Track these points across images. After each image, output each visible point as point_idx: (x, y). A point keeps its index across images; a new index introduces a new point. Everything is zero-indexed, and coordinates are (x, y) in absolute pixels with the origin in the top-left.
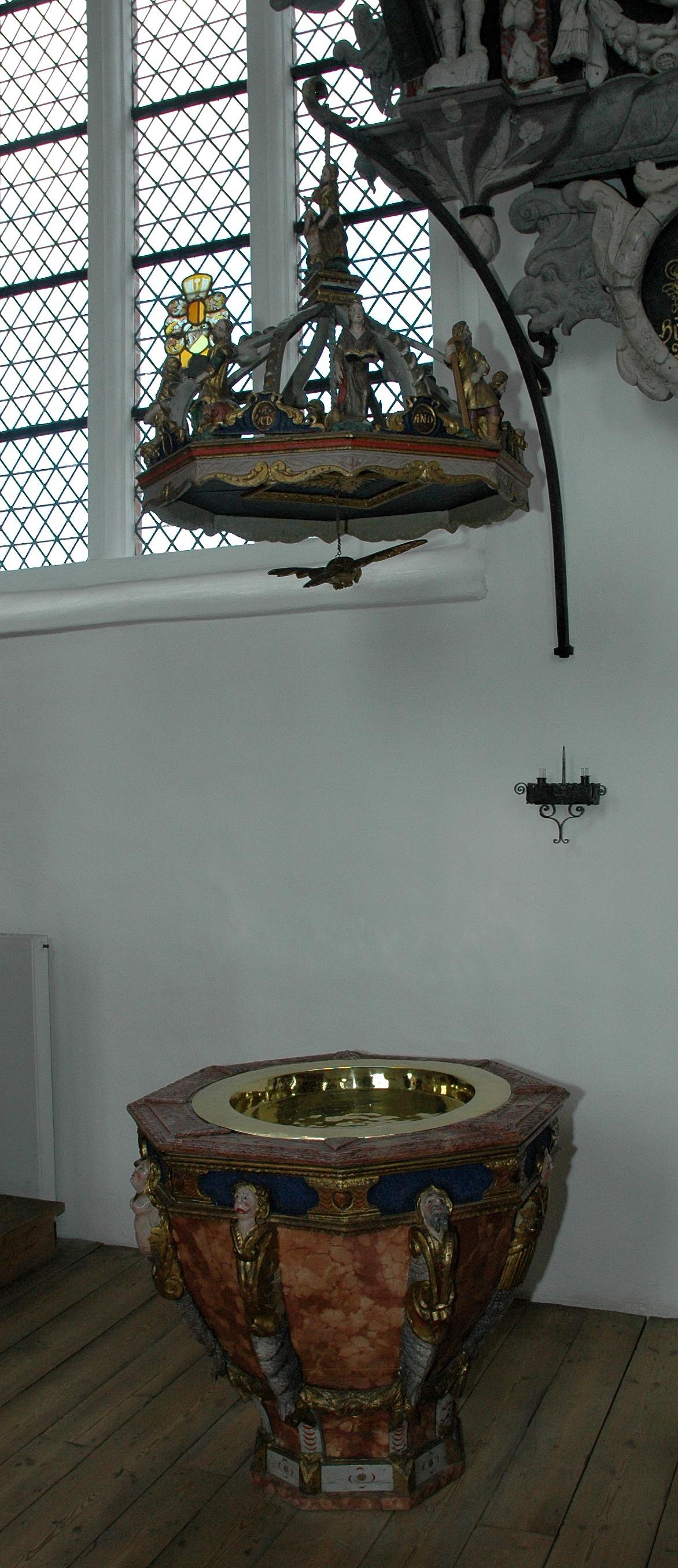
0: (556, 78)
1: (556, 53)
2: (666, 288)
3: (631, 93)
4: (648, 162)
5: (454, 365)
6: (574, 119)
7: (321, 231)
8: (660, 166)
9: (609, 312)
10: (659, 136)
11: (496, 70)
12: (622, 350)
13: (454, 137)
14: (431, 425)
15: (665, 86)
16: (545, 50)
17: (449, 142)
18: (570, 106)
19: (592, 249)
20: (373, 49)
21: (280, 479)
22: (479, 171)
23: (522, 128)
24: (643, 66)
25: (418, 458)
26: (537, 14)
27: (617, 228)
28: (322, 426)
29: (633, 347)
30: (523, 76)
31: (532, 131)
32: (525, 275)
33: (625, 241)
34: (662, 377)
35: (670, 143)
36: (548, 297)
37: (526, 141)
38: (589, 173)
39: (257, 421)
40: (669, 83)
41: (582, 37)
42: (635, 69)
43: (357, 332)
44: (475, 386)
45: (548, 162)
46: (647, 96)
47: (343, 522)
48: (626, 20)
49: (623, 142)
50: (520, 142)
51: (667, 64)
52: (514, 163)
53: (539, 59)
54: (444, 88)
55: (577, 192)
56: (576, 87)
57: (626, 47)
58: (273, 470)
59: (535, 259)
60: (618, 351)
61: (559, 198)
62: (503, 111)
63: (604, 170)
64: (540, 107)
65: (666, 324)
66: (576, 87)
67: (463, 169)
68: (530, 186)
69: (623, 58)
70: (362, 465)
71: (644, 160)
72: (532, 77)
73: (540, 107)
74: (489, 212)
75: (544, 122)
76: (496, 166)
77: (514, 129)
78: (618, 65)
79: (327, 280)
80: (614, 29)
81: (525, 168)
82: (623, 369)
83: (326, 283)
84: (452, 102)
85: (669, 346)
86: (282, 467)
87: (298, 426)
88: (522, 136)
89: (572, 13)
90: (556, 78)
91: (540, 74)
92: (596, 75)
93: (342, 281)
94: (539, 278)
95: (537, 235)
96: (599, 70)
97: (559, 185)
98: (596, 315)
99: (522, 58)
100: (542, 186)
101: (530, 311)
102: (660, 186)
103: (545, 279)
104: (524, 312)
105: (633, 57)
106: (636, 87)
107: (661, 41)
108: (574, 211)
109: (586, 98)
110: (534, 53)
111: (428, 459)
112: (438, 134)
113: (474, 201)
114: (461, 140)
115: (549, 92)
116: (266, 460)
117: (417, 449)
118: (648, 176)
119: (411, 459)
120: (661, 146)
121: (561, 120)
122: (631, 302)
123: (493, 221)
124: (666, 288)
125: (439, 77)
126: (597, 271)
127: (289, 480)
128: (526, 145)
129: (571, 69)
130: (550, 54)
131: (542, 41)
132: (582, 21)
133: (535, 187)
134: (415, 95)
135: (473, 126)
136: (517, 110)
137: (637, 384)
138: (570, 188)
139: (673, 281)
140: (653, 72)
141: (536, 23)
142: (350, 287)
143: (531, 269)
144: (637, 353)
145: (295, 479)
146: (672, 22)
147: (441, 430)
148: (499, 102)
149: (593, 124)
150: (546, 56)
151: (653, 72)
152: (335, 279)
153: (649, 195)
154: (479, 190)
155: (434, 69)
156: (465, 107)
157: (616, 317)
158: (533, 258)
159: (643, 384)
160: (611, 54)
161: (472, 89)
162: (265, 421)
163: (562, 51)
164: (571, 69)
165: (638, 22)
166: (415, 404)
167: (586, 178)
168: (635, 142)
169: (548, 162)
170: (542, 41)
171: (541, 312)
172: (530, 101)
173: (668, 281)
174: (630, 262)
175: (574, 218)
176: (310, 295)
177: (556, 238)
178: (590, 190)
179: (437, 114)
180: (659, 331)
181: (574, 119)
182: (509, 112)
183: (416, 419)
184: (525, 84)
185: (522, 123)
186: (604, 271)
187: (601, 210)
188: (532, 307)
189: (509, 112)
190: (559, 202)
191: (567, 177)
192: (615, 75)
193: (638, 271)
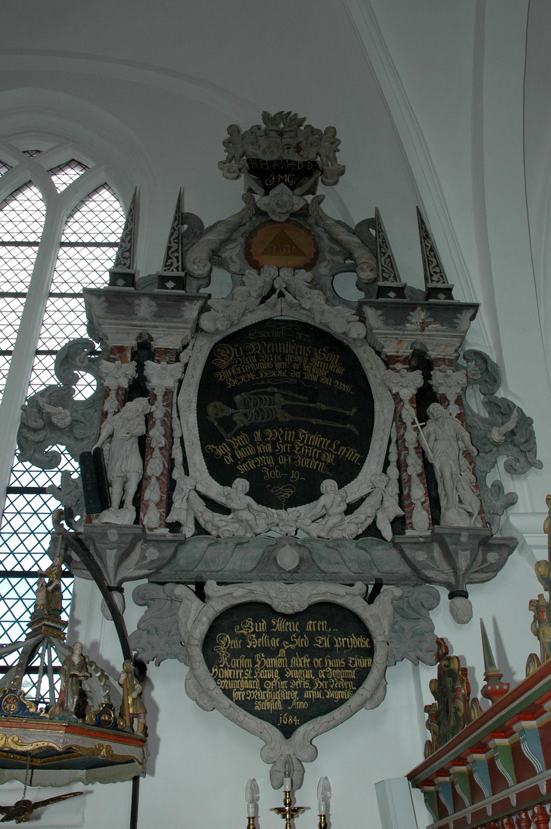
0: (168, 530)
1: (169, 517)
2: (216, 648)
3: (206, 545)
4: (213, 581)
5: (125, 686)
6: (175, 552)
7: (47, 592)
8: (219, 584)
9: (183, 657)
10: (219, 568)
11: (137, 521)
12: (189, 679)
13: (112, 549)
14: (110, 722)
15: (224, 545)
16: (164, 514)
17: (108, 551)
18: (176, 544)
19: (177, 622)
20: (69, 493)
21: (13, 746)
22: (121, 568)
23: (148, 551)
24: (214, 533)
25: (101, 742)
26: (162, 497)
27: (193, 612)
28: (47, 716)
29: (196, 678)
30: (152, 525)
31: (153, 553)
32: (136, 629)
33: (197, 620)
34: (211, 697)
35: (224, 573)
36: (150, 644)
37: (149, 558)
38: (180, 580)
39: (5, 706)
40: (226, 543)
41: (184, 513)
42: (208, 533)
43: (76, 659)
44: (134, 700)
45: (159, 570)
46: (214, 547)
47: (30, 771)
48: (207, 510)
49: (200, 568)
50: (145, 558)
51: (226, 534)
52: (140, 568)
53: (160, 519)
54: (110, 523)
55: (172, 590)
56: (178, 537)
57: (206, 522)
58: (10, 740)
59: (144, 621)
60: (186, 679)
61: (162, 590)
62: (139, 540)
63: (188, 580)
64: (158, 542)
65: (215, 668)
66: (178, 537)
67: (113, 566)
68: (146, 581)
69: (203, 527)
70: (68, 745)
71: (211, 579)
72: (156, 527)
73: (158, 542)
74: (121, 590)
75: (160, 550)
76: (130, 567)
77: (143, 551)
78: (200, 530)
79: (48, 621)
80: (201, 512)
81: (146, 572)
82: (187, 687)
83: (47, 623)
84: (114, 531)
85: (216, 680)
86: (16, 739)
87: (32, 714)
88: (147, 555)
89: (180, 500)
90: (168, 530)
91: (160, 526)
92: (189, 530)
93: (57, 623)
94: (145, 632)
95: (146, 608)
96: (190, 530)
97: (162, 584)
98: (176, 657)
99: (152, 517)
100: (153, 582)
101: (138, 650)
102: (218, 594)
103: (148, 632)
104: (134, 650)
105: (209, 528)
106: (210, 542)
107: (225, 523)
108: (169, 599)
109: (184, 542)
110: (159, 515)
111: (106, 743)
112: (103, 545)
113: (115, 584)
114: (115, 551)
115: (165, 536)
116: (6, 733)
117: (102, 736)
118: (211, 588)
119: (98, 741)
120: (220, 573)
121: (169, 552)
122: (197, 653)
123: (123, 596)
124: (216, 648)
125: (109, 517)
126: (178, 633)
127: (19, 749)
128: (149, 560)
129: (175, 527)
130: (166, 517)
131: (163, 510)
132: (185, 506)
133: (149, 582)
134: (91, 523)
135: (123, 545)
136: (146, 541)
137: (196, 700)
138: (167, 586)
139: (221, 645)
140: (218, 537)
141: (161, 500)
142: (60, 627)
143: (142, 626)
144: (198, 682)
145: (24, 749)
146: (231, 516)
147: (115, 726)
148: (139, 535)
149: (185, 556)
150: (164, 518)
151: (218, 537)
152: (53, 621)
153: (212, 597)
154: (119, 579)
155: (105, 512)
156: (121, 535)
157: (188, 660)
158: (142, 621)
159: (198, 699)
160: (197, 523)
161: (125, 527)
162: (10, 707)
163: (172, 518)
164: (175, 527)
165: (213, 512)
166: (104, 708)
167: (178, 583)
168: (206, 569)
169: (159, 570)
170: (163, 510)
171: (144, 651)
172: (154, 538)
173: (218, 645)
174: (200, 631)
175: (169, 603)
176: (35, 627)
177: (157, 611)
178: (180, 590)
179: (104, 535)
180: (211, 672)
181: (175, 552)
182: (142, 541)
183: (103, 718)
184: (151, 529)
185: (148, 548)
186: (183, 634)
187: (185, 601)
188: (140, 648)
189: (142, 541)
190: (161, 593)
191: (168, 581)
192: (198, 534)
193: (203, 637)
